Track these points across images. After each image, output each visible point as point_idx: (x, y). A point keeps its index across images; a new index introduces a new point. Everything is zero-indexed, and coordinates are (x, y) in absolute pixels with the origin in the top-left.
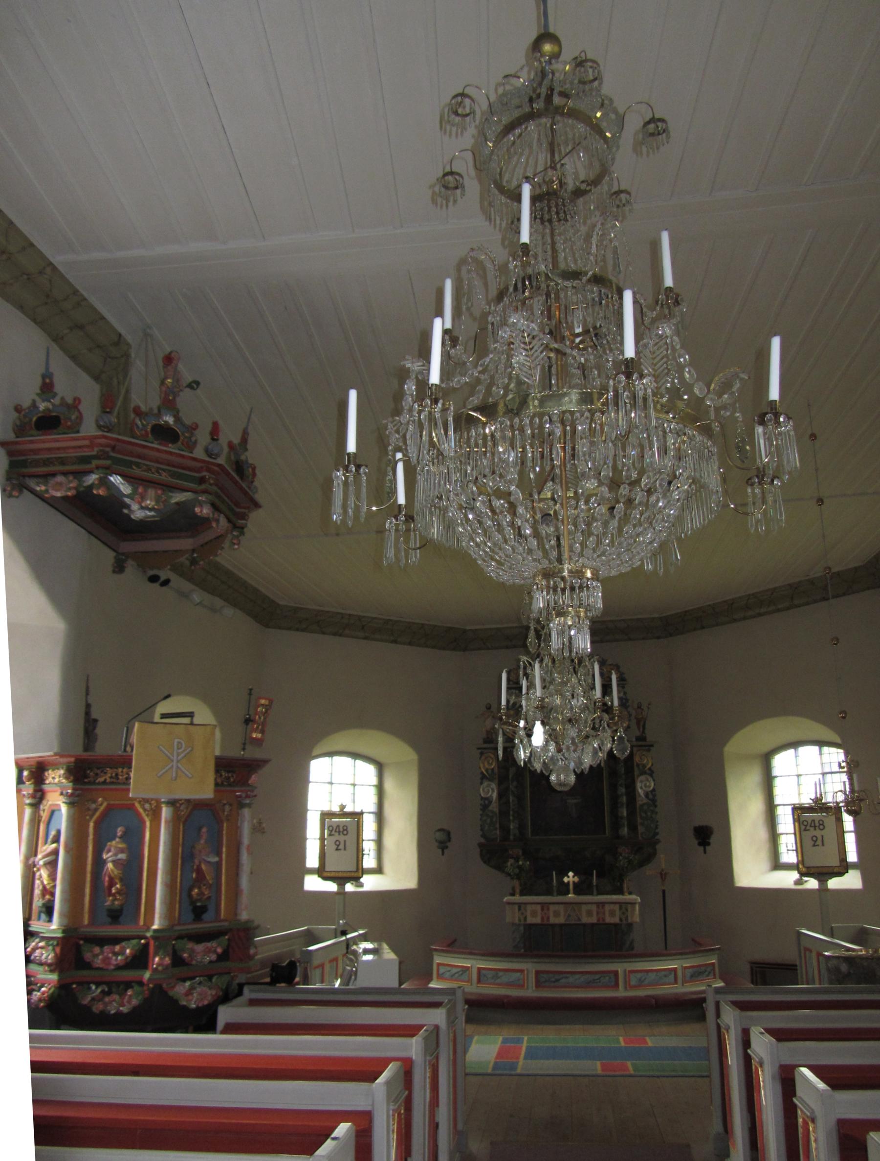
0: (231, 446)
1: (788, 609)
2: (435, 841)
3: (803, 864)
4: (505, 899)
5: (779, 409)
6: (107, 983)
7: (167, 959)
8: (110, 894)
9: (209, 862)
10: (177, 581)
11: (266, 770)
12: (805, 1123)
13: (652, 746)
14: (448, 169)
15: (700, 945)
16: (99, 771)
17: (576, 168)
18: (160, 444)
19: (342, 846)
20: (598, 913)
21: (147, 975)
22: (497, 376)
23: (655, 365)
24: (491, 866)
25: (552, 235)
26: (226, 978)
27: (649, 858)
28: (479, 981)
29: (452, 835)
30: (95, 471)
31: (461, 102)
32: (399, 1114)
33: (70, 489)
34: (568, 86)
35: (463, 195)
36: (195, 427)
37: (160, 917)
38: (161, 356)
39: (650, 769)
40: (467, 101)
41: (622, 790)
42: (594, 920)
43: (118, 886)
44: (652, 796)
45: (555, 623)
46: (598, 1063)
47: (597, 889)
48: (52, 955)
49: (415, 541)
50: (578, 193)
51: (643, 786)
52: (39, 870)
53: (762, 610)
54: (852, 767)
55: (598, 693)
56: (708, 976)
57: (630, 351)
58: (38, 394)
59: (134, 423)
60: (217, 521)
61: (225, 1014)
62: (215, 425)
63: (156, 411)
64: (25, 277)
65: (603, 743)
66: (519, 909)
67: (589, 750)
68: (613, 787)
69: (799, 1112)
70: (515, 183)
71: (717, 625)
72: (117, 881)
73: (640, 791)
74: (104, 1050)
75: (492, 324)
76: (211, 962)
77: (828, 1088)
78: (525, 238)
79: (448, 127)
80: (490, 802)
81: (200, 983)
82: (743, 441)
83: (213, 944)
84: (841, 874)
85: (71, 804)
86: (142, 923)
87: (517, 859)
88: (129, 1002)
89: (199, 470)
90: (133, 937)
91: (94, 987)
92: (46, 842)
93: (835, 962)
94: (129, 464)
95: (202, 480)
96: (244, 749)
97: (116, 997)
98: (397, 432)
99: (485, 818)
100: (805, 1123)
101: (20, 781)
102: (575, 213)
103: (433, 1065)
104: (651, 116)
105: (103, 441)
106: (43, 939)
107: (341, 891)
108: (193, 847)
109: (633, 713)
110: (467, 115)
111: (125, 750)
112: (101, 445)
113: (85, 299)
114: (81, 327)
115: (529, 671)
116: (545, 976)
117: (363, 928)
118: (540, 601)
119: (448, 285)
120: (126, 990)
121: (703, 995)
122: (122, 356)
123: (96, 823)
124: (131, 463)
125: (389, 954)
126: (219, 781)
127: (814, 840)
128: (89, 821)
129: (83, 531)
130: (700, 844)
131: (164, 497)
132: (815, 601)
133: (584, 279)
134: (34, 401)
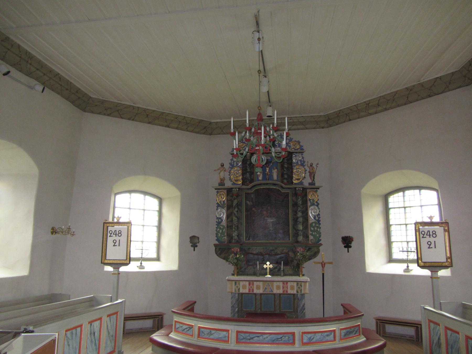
4: (227, 278)
13: (318, 189)
19: (117, 244)
20: (283, 287)
24: (221, 258)
27: (316, 254)
28: (199, 336)
39: (317, 202)
41: (300, 214)
42: (281, 291)
56: (355, 333)
66: (236, 284)
68: (295, 212)
71: (359, 118)
84: (127, 264)
99: (218, 230)
107: (116, 272)
109: (308, 169)
116: (243, 334)
127: (429, 244)
130: (345, 247)
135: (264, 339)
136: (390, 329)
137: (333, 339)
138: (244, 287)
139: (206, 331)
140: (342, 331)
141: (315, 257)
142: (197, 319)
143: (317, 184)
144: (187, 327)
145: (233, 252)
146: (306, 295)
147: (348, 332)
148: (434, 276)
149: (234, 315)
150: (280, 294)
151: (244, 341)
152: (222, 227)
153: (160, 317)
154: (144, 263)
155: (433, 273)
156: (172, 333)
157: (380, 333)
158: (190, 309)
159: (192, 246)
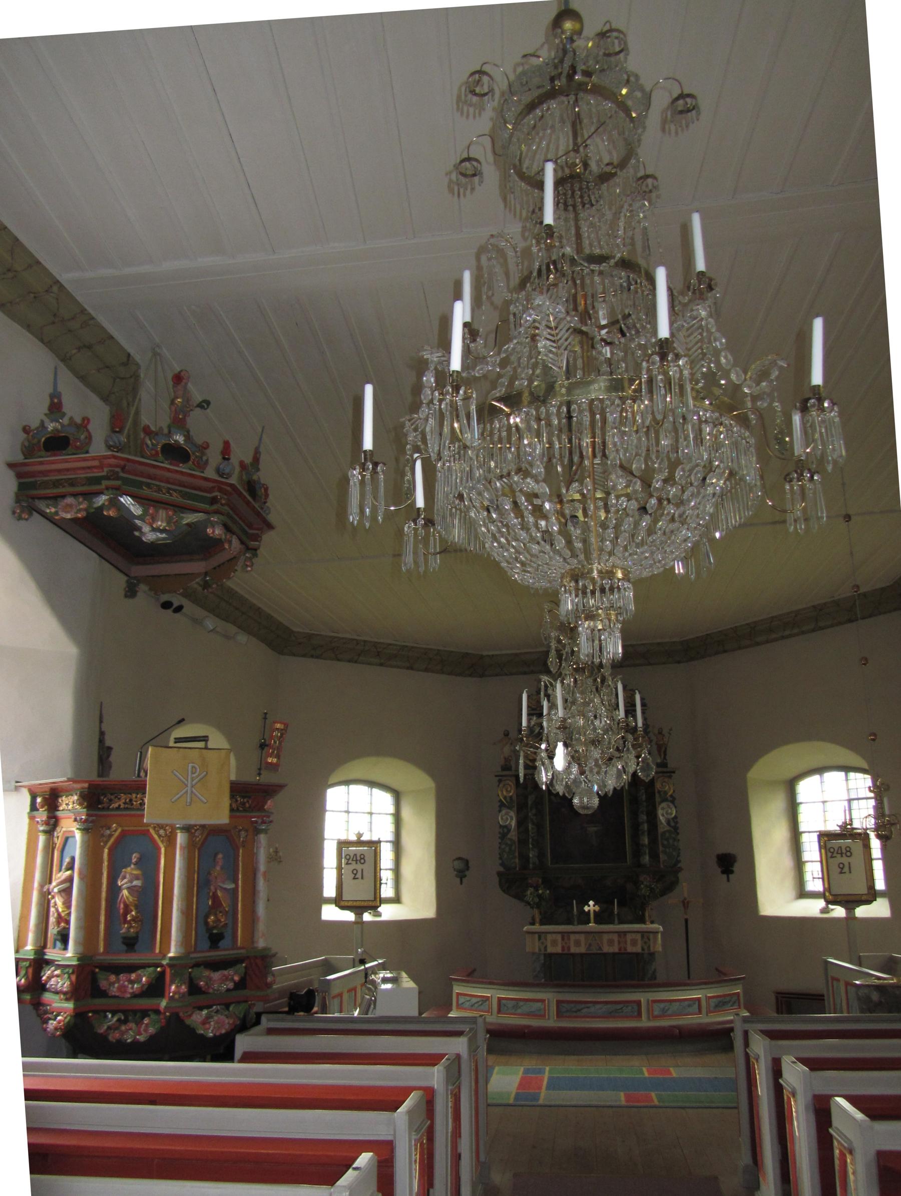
0: (242, 465)
1: (813, 630)
2: (453, 869)
3: (830, 892)
4: (525, 929)
5: (823, 395)
6: (124, 1012)
7: (183, 987)
8: (125, 921)
9: (225, 889)
10: (189, 607)
11: (280, 797)
12: (843, 1155)
13: (674, 772)
14: (465, 155)
15: (725, 974)
16: (112, 797)
17: (601, 151)
18: (171, 464)
19: (359, 875)
21: (164, 1003)
22: (519, 370)
23: (689, 350)
25: (577, 220)
26: (242, 1007)
27: (670, 888)
28: (499, 1011)
29: (470, 864)
30: (105, 492)
31: (479, 81)
32: (422, 1144)
33: (79, 511)
34: (591, 62)
35: (481, 182)
36: (205, 446)
37: (176, 945)
38: (170, 376)
39: (671, 796)
40: (485, 79)
42: (615, 949)
43: (133, 913)
44: (674, 824)
45: (585, 626)
46: (622, 1094)
47: (619, 919)
48: (67, 983)
49: (435, 545)
50: (605, 177)
51: (664, 813)
52: (53, 897)
53: (787, 633)
54: (880, 791)
55: (621, 713)
57: (664, 332)
58: (46, 415)
59: (143, 442)
60: (230, 542)
61: (243, 1043)
62: (227, 444)
63: (166, 431)
64: (32, 295)
65: (626, 763)
66: (540, 938)
67: (613, 771)
68: (635, 814)
69: (835, 1143)
70: (535, 168)
71: (740, 648)
72: (133, 908)
73: (661, 818)
74: (117, 1079)
75: (514, 315)
76: (228, 990)
77: (867, 1119)
78: (549, 218)
79: (465, 109)
80: (509, 831)
81: (217, 1012)
82: (781, 432)
83: (229, 972)
84: (868, 902)
85: (85, 830)
86: (157, 951)
87: (536, 888)
88: (146, 1030)
89: (210, 491)
90: (149, 966)
91: (110, 1016)
92: (60, 870)
93: (866, 991)
94: (140, 485)
95: (214, 501)
96: (259, 774)
97: (132, 1025)
98: (415, 430)
99: (503, 846)
100: (843, 1155)
101: (33, 807)
102: (600, 197)
103: (455, 1095)
104: (680, 92)
105: (112, 461)
106: (59, 967)
108: (209, 873)
110: (485, 94)
111: (139, 776)
112: (110, 466)
113: (93, 318)
114: (89, 347)
115: (550, 692)
116: (565, 1005)
117: (380, 958)
118: (569, 603)
119: (467, 277)
120: (143, 1018)
121: (732, 1025)
122: (131, 377)
123: (110, 850)
124: (142, 483)
125: (407, 983)
126: (234, 806)
127: (841, 867)
128: (104, 848)
129: (95, 555)
130: (723, 872)
131: (175, 518)
132: (840, 623)
133: (612, 262)
134: (42, 422)
138: (554, 943)
143: (671, 765)
144: (479, 999)
152: (509, 842)
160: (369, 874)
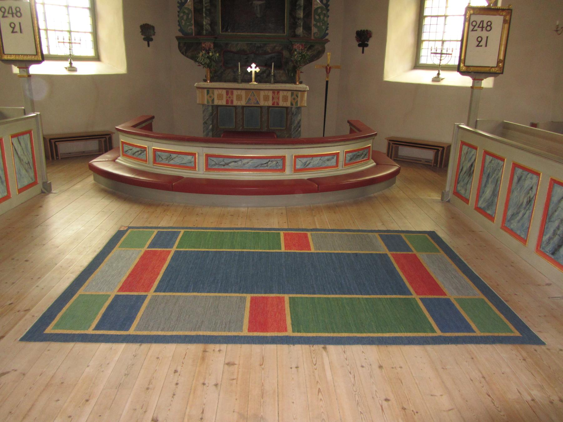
4: (196, 84)
20: (273, 98)
24: (187, 57)
27: (319, 54)
28: (155, 161)
42: (270, 103)
66: (208, 93)
84: (39, 62)
99: (182, 15)
107: (25, 74)
127: (479, 41)
130: (359, 45)
135: (244, 164)
136: (404, 152)
137: (334, 164)
139: (164, 155)
140: (348, 154)
141: (318, 58)
142: (150, 139)
145: (204, 49)
146: (302, 108)
147: (355, 155)
148: (476, 85)
149: (207, 134)
150: (269, 107)
151: (216, 167)
152: (186, 11)
153: (107, 137)
154: (75, 64)
155: (476, 81)
156: (119, 158)
157: (391, 155)
158: (146, 127)
159: (144, 39)
160: (27, 28)
